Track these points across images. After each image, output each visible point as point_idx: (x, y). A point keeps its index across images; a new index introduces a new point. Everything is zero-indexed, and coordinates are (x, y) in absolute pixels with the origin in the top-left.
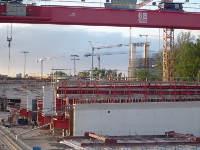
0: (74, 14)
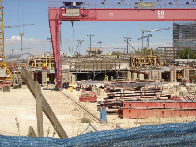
0: (113, 14)
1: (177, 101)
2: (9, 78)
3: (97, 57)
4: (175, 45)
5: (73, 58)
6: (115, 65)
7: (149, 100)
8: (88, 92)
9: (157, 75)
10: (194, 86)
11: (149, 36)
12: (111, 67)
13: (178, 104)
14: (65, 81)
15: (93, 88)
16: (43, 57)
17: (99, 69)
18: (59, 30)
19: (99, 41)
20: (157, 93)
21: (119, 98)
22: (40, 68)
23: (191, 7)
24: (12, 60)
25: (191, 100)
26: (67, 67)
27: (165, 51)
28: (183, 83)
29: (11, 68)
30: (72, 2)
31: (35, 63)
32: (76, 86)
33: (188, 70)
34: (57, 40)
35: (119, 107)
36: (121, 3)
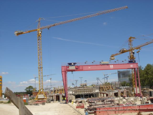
1: (122, 106)
2: (45, 99)
3: (84, 87)
4: (119, 80)
5: (74, 88)
6: (93, 91)
7: (109, 106)
8: (80, 104)
9: (112, 94)
10: (129, 99)
11: (107, 77)
12: (91, 91)
13: (122, 107)
14: (70, 99)
15: (83, 102)
16: (60, 88)
17: (86, 93)
18: (66, 76)
19: (85, 80)
20: (112, 103)
21: (94, 106)
22: (59, 94)
23: (124, 63)
24: (47, 90)
25: (128, 105)
26: (71, 93)
27: (115, 83)
28: (124, 97)
29: (46, 94)
30: (72, 63)
31: (57, 92)
32: (75, 101)
33: (126, 91)
34: (66, 80)
35: (95, 110)
36: (94, 62)
